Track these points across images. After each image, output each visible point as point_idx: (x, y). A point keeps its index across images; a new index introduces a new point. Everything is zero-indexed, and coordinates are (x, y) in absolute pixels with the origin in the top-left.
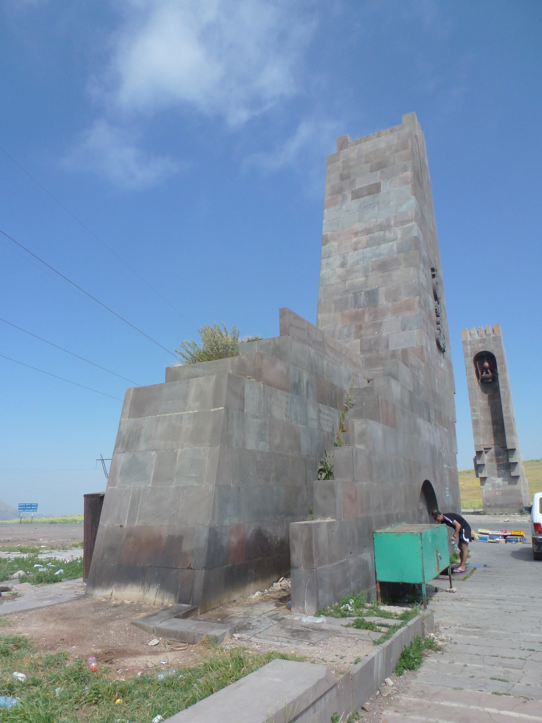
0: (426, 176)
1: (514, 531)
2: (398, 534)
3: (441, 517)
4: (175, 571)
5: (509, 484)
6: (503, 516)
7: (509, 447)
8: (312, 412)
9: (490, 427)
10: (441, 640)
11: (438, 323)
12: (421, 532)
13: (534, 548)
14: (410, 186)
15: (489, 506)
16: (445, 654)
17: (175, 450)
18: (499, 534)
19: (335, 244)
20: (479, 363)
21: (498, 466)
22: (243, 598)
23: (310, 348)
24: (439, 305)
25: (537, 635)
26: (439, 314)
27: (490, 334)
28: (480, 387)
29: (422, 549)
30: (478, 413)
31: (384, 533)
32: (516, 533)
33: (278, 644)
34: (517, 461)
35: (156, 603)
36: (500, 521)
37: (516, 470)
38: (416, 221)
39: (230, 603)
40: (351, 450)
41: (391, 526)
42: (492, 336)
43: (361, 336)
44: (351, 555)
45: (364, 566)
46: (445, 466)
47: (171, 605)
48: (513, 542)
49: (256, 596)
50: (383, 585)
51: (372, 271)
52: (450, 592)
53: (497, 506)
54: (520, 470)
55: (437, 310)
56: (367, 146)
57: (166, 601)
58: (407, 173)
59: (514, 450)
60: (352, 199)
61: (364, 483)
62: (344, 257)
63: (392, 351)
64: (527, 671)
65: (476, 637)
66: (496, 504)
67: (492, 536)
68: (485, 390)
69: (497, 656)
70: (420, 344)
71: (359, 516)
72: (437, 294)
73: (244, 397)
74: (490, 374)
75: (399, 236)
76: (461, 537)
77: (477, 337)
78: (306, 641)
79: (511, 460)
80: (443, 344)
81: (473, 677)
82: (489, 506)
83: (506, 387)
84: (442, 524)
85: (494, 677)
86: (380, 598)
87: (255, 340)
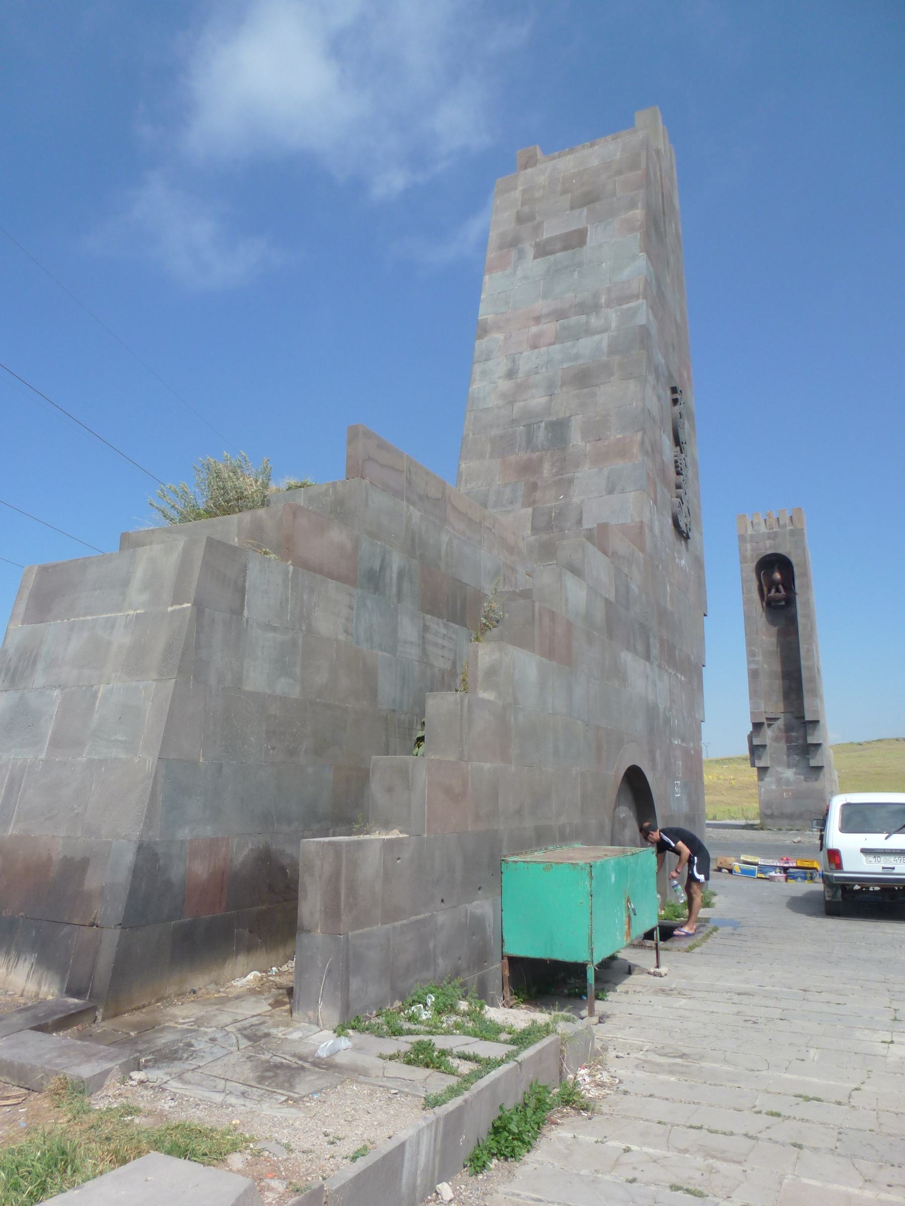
0: (674, 226)
1: (802, 861)
2: (548, 866)
3: (656, 835)
4: (66, 929)
5: (806, 780)
6: (792, 834)
7: (808, 717)
8: (408, 630)
9: (778, 684)
10: (599, 1085)
11: (678, 487)
12: (592, 863)
13: (826, 894)
14: (638, 235)
15: (771, 816)
16: (596, 1119)
17: (95, 687)
18: (775, 864)
19: (499, 336)
20: (764, 574)
21: (789, 748)
22: (216, 984)
23: (412, 507)
24: (683, 454)
25: (795, 1077)
26: (681, 470)
27: (785, 526)
28: (764, 614)
29: (591, 896)
30: (759, 658)
31: (522, 863)
32: (806, 864)
33: (218, 1098)
34: (820, 742)
35: (25, 993)
36: (786, 842)
37: (818, 757)
38: (645, 297)
39: (180, 995)
40: (459, 700)
41: (546, 849)
42: (789, 528)
43: (534, 502)
44: (443, 905)
45: (476, 925)
46: (676, 743)
47: (50, 998)
48: (799, 879)
49: (248, 981)
50: (514, 962)
51: (561, 386)
52: (655, 975)
53: (783, 816)
54: (829, 757)
55: (679, 463)
56: (567, 164)
57: (44, 988)
58: (636, 211)
59: (817, 722)
60: (535, 258)
61: (487, 766)
62: (514, 361)
63: (587, 529)
64: (753, 1169)
65: (673, 1079)
67: (763, 869)
68: (772, 621)
69: (701, 1128)
70: (638, 520)
71: (470, 829)
72: (680, 434)
73: (244, 587)
74: (783, 593)
75: (614, 325)
76: (690, 872)
77: (763, 529)
78: (282, 1094)
79: (811, 740)
80: (686, 525)
81: (633, 1181)
82: (771, 816)
83: (809, 616)
84: (643, 849)
85: (679, 1183)
86: (507, 988)
87: (300, 487)
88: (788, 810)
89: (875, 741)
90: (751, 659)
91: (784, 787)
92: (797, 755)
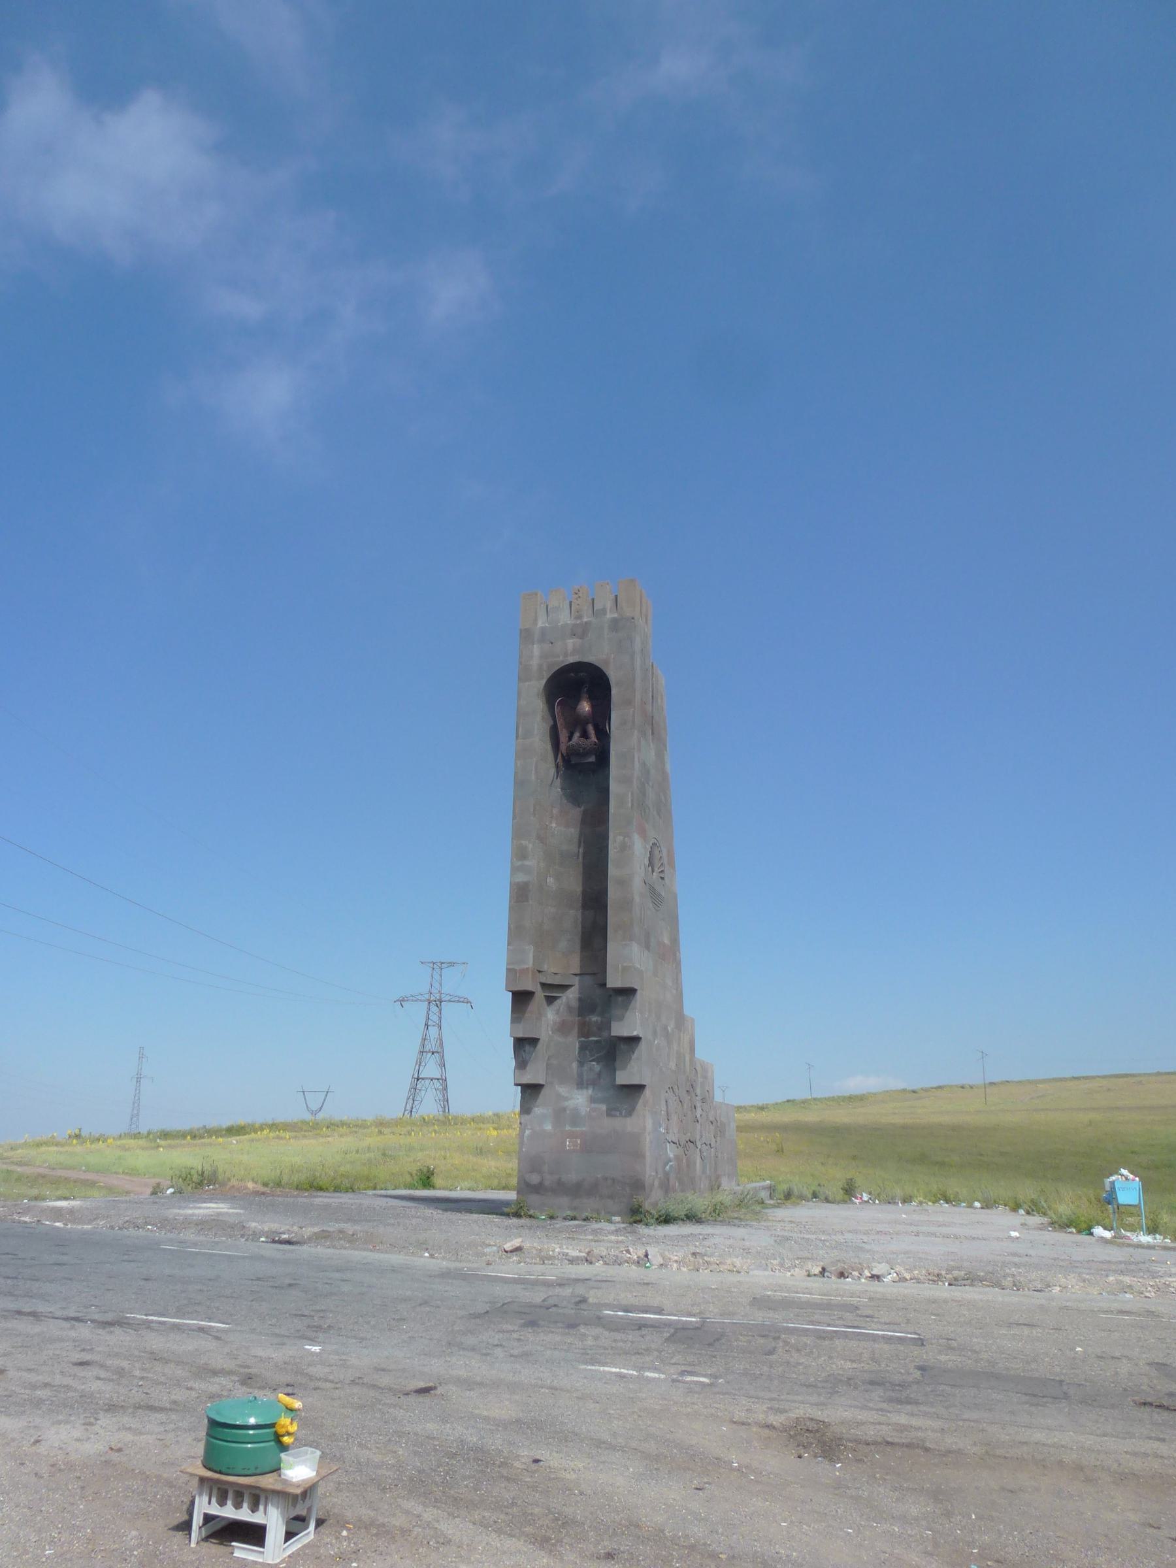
7: (614, 980)
15: (537, 1189)
21: (583, 1048)
27: (604, 611)
28: (558, 782)
34: (635, 1033)
66: (560, 1180)
68: (574, 798)
74: (593, 738)
79: (620, 1029)
82: (537, 1189)
88: (572, 1177)
89: (935, 1088)
90: (519, 863)
91: (568, 1128)
92: (598, 1061)
